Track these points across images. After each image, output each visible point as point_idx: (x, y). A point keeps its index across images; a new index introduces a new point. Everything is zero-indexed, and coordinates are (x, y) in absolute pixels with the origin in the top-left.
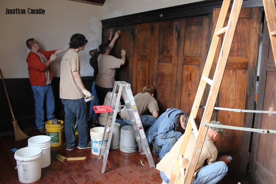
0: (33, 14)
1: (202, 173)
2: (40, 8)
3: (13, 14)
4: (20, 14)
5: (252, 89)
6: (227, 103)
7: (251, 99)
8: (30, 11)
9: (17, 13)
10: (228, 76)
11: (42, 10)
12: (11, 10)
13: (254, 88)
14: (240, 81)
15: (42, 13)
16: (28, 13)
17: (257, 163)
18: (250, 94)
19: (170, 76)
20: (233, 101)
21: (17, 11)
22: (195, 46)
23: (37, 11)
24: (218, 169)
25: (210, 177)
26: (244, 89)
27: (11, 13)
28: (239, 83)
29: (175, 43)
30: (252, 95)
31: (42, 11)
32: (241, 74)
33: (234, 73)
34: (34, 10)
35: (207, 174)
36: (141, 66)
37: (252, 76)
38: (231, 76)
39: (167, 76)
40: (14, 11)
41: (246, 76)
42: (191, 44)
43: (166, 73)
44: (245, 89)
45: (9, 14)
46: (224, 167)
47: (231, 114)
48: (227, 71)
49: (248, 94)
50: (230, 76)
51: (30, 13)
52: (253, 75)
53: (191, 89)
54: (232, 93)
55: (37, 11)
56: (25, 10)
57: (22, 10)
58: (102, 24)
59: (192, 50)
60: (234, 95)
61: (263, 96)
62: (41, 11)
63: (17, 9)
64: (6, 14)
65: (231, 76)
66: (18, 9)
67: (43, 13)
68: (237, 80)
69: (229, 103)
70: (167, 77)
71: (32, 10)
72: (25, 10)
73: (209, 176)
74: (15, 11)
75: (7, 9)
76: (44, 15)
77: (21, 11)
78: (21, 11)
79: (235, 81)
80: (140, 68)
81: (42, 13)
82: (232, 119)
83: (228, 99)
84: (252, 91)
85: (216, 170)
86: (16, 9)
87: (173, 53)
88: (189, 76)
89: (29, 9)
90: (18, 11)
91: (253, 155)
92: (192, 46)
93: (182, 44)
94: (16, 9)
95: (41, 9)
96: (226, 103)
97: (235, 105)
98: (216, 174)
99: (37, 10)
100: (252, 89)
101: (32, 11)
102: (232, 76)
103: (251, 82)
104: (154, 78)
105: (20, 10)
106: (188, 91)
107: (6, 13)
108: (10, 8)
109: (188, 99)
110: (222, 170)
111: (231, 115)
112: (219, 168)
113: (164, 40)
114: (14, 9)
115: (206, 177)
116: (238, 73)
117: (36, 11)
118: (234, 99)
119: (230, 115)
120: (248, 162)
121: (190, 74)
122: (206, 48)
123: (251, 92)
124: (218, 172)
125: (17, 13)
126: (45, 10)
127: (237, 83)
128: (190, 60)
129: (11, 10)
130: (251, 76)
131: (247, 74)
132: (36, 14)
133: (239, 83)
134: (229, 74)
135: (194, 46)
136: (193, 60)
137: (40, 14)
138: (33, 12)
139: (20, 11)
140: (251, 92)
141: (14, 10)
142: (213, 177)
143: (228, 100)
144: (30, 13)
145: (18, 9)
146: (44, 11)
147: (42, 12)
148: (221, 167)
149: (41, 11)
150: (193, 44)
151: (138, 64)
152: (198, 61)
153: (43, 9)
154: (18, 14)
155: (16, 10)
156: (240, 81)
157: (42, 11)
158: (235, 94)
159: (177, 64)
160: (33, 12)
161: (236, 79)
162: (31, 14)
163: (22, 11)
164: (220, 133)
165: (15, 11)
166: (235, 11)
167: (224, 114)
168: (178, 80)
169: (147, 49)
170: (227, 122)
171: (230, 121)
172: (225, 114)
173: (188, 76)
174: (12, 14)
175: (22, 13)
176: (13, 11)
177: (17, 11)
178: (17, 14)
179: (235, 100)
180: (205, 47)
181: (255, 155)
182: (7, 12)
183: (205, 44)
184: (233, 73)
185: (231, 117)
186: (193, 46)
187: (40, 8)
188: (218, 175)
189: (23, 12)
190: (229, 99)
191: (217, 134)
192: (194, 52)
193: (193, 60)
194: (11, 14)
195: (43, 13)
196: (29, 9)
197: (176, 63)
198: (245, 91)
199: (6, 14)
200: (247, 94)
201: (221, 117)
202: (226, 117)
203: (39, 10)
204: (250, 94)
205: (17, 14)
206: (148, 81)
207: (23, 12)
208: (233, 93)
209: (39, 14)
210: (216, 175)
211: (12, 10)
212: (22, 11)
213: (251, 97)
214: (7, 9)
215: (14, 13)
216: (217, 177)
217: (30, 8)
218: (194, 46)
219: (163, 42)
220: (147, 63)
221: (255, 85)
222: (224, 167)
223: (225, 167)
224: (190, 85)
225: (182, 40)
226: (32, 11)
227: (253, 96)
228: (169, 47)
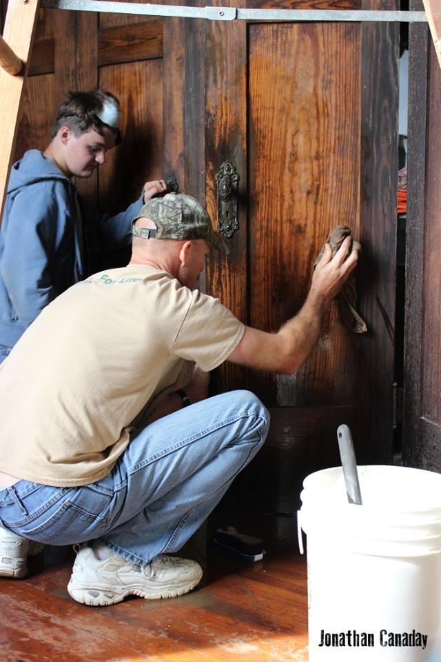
0: (395, 647)
1: (147, 443)
3: (341, 645)
4: (358, 645)
5: (386, 102)
6: (286, 171)
7: (384, 147)
8: (386, 638)
9: (352, 643)
10: (283, 55)
11: (419, 634)
12: (333, 635)
13: (390, 102)
14: (331, 73)
15: (420, 645)
16: (381, 644)
17: (423, 418)
18: (379, 125)
20: (312, 162)
21: (352, 637)
23: (406, 638)
24: (223, 419)
25: (189, 458)
26: (350, 105)
27: (335, 643)
28: (331, 81)
30: (386, 131)
31: (420, 638)
32: (334, 41)
33: (307, 38)
34: (396, 635)
35: (172, 446)
37: (380, 45)
38: (293, 51)
40: (344, 639)
41: (357, 47)
44: (355, 104)
46: (250, 406)
47: (306, 219)
48: (277, 31)
49: (370, 125)
50: (290, 54)
51: (386, 642)
52: (385, 41)
54: (303, 128)
55: (406, 638)
56: (373, 635)
57: (365, 634)
60: (314, 134)
61: (423, 119)
62: (416, 638)
63: (352, 633)
64: (321, 645)
65: (293, 51)
66: (354, 632)
67: (422, 643)
68: (321, 68)
69: (294, 173)
71: (392, 634)
73: (179, 453)
74: (346, 638)
75: (323, 631)
76: (425, 649)
77: (361, 638)
78: (361, 638)
79: (312, 73)
81: (420, 645)
82: (311, 241)
83: (288, 155)
84: (385, 112)
85: (211, 426)
86: (349, 632)
89: (383, 633)
91: (409, 389)
94: (349, 632)
95: (416, 633)
96: (282, 174)
97: (318, 180)
98: (215, 442)
100: (386, 102)
101: (392, 638)
102: (297, 53)
103: (376, 73)
105: (358, 635)
108: (331, 630)
110: (238, 423)
111: (306, 225)
112: (227, 414)
115: (167, 460)
116: (321, 38)
117: (402, 638)
118: (313, 154)
119: (302, 222)
120: (395, 427)
123: (383, 117)
124: (219, 434)
125: (352, 643)
126: (426, 636)
127: (323, 80)
129: (335, 636)
130: (375, 47)
131: (360, 43)
132: (404, 645)
133: (331, 81)
134: (284, 43)
137: (414, 645)
139: (358, 639)
140: (380, 119)
141: (343, 634)
142: (201, 457)
143: (288, 160)
144: (386, 642)
145: (354, 632)
147: (420, 642)
148: (236, 410)
149: (416, 638)
153: (422, 634)
154: (354, 645)
155: (349, 634)
156: (331, 73)
157: (420, 638)
158: (318, 130)
161: (317, 64)
162: (390, 645)
164: (197, 237)
165: (346, 638)
167: (276, 220)
171: (307, 253)
172: (282, 223)
175: (366, 645)
177: (352, 637)
178: (350, 645)
179: (317, 157)
181: (416, 387)
182: (322, 641)
184: (302, 40)
185: (309, 230)
187: (414, 631)
188: (222, 446)
189: (368, 640)
190: (294, 155)
191: (189, 246)
194: (333, 645)
195: (422, 643)
196: (383, 633)
198: (356, 114)
199: (321, 645)
200: (364, 126)
201: (267, 235)
202: (286, 232)
203: (410, 635)
204: (379, 125)
205: (350, 645)
207: (368, 640)
208: (309, 125)
209: (411, 645)
210: (212, 447)
212: (365, 638)
213: (383, 138)
214: (323, 631)
216: (220, 457)
221: (393, 86)
222: (250, 406)
223: (252, 408)
226: (392, 638)
227: (390, 133)
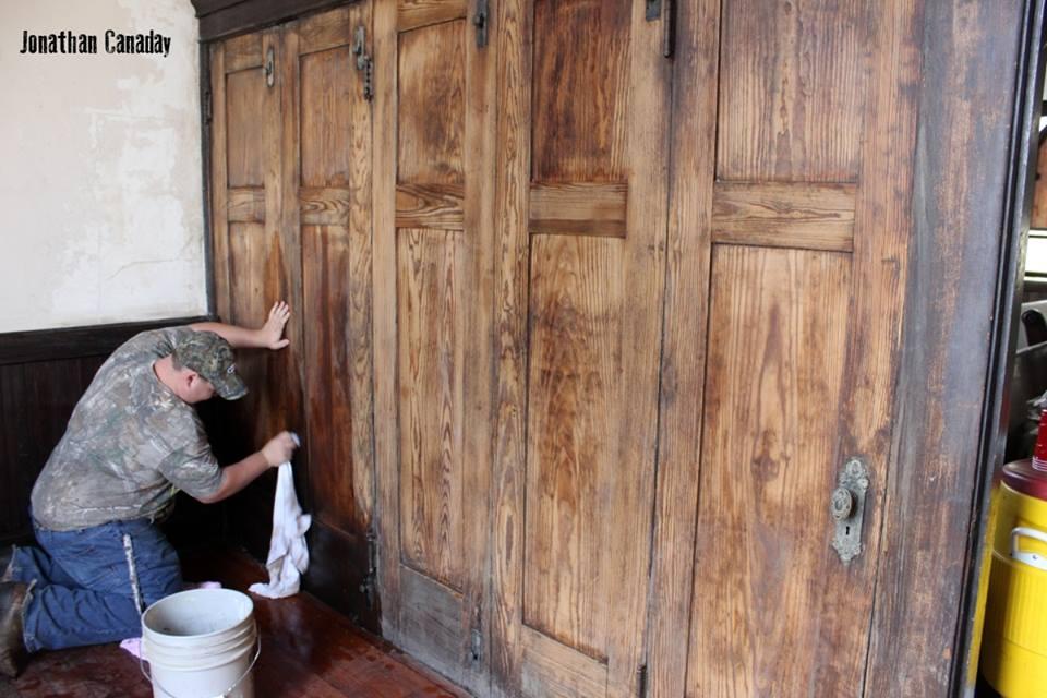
0: (125, 54)
2: (152, 32)
4: (75, 52)
8: (113, 42)
9: (66, 49)
11: (160, 36)
15: (161, 51)
16: (107, 49)
19: (614, 327)
21: (66, 40)
22: (808, 105)
23: (141, 42)
27: (43, 49)
29: (642, 92)
31: (160, 42)
36: (417, 256)
39: (596, 327)
40: (54, 42)
42: (771, 91)
43: (594, 304)
45: (33, 51)
53: (778, 426)
55: (141, 42)
56: (95, 38)
57: (84, 36)
58: (197, 21)
59: (784, 136)
62: (155, 41)
63: (66, 34)
64: (23, 52)
66: (70, 33)
67: (163, 49)
70: (590, 334)
71: (122, 36)
72: (95, 38)
74: (58, 41)
75: (26, 32)
77: (78, 42)
78: (78, 42)
80: (416, 271)
81: (161, 51)
86: (62, 33)
87: (638, 155)
88: (765, 327)
89: (110, 34)
90: (70, 41)
92: (783, 108)
93: (701, 95)
94: (62, 33)
95: (155, 34)
99: (142, 36)
101: (122, 42)
104: (506, 340)
105: (75, 38)
106: (755, 436)
107: (22, 48)
108: (37, 31)
109: (759, 491)
113: (565, 78)
114: (53, 33)
117: (136, 42)
121: (766, 315)
122: (906, 112)
125: (66, 49)
128: (772, 214)
135: (800, 108)
136: (796, 214)
137: (152, 52)
138: (126, 44)
139: (75, 43)
141: (54, 36)
145: (70, 33)
146: (167, 42)
147: (160, 47)
149: (155, 41)
150: (792, 88)
151: (404, 248)
152: (837, 215)
153: (163, 36)
154: (70, 52)
155: (62, 37)
157: (160, 42)
159: (664, 247)
160: (126, 44)
162: (119, 52)
163: (84, 42)
165: (58, 41)
166: (385, 343)
168: (679, 355)
169: (453, 146)
170: (757, 312)
173: (750, 325)
174: (45, 52)
175: (85, 51)
176: (49, 42)
177: (66, 40)
180: (899, 109)
182: (25, 46)
183: (901, 88)
186: (790, 105)
187: (152, 32)
189: (89, 44)
192: (796, 153)
193: (796, 214)
194: (40, 52)
195: (163, 49)
196: (110, 34)
197: (660, 235)
199: (23, 52)
203: (147, 37)
205: (63, 52)
206: (466, 355)
207: (89, 44)
209: (147, 52)
211: (45, 37)
212: (84, 42)
214: (26, 32)
215: (55, 51)
217: (112, 32)
218: (800, 108)
219: (555, 94)
220: (457, 235)
224: (776, 399)
225: (702, 65)
226: (122, 42)
228: (603, 125)
